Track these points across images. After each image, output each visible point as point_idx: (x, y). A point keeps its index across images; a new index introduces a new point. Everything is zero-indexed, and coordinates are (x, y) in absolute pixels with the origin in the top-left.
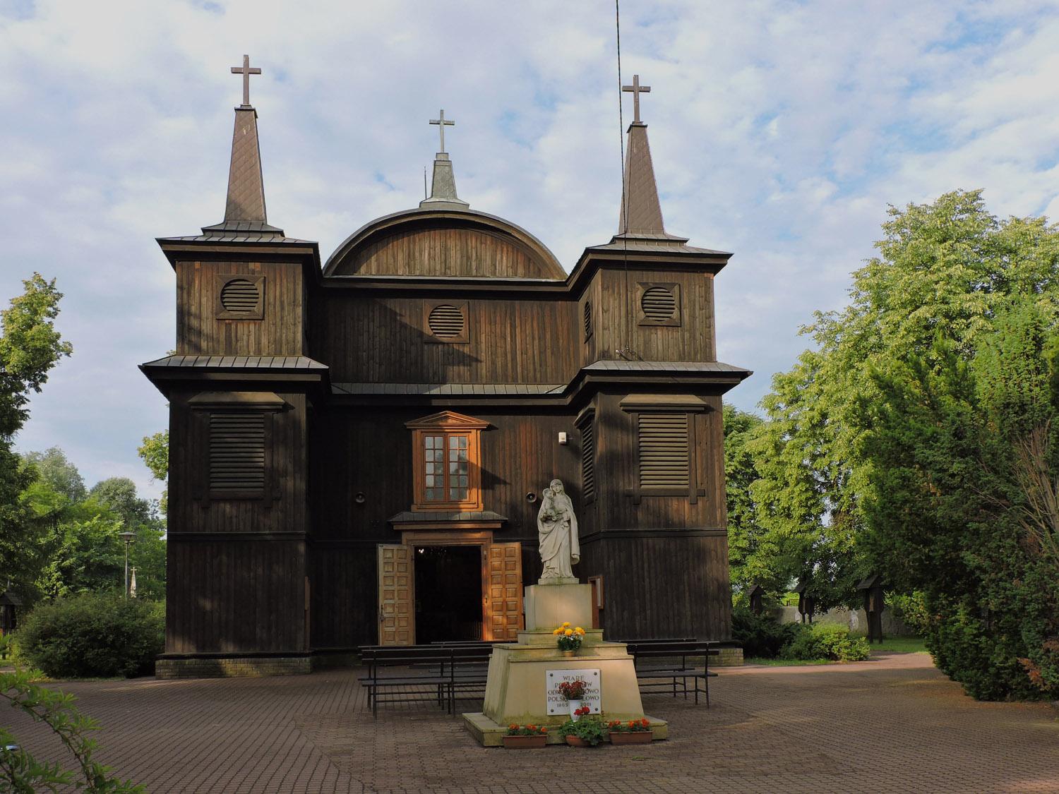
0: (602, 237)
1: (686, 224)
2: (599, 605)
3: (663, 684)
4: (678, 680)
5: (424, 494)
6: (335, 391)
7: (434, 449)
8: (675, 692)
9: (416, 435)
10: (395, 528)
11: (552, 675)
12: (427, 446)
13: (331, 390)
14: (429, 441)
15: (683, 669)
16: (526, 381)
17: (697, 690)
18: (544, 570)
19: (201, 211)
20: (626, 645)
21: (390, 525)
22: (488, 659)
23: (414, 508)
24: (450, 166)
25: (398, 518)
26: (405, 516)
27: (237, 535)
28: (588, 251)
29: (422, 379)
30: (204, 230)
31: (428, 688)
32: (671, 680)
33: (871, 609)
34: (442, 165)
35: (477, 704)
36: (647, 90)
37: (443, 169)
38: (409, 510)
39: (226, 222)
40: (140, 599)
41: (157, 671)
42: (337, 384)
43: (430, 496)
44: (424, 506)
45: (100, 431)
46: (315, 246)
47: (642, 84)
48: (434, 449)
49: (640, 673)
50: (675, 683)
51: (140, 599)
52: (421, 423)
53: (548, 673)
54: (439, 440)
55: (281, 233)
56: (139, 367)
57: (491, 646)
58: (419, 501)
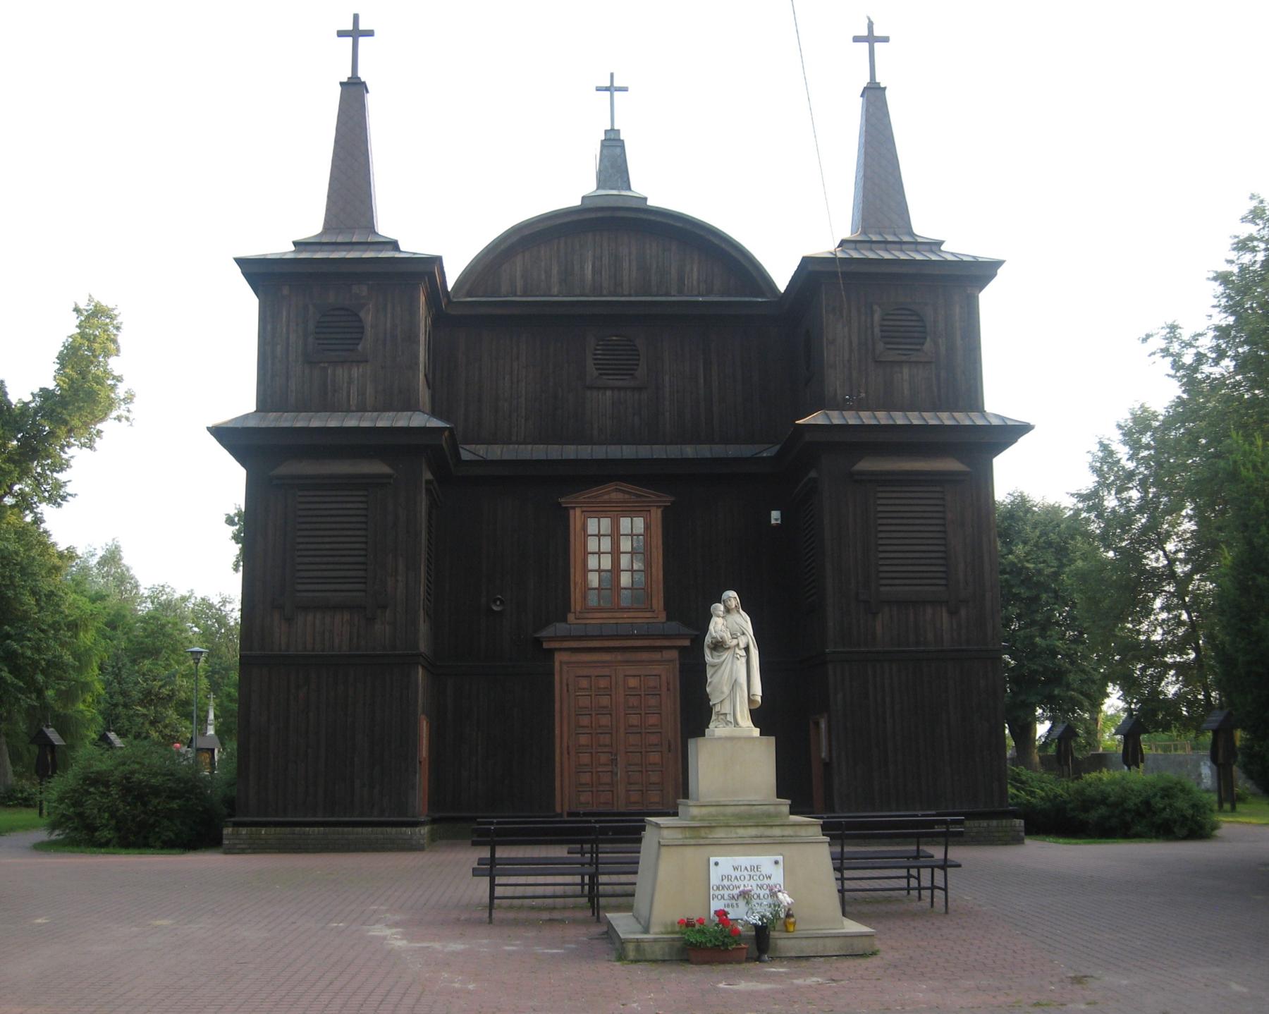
0: (824, 244)
1: (942, 217)
2: (823, 755)
3: (864, 880)
4: (914, 872)
5: (585, 598)
6: (465, 455)
7: (632, 535)
8: (909, 889)
9: (576, 516)
10: (545, 645)
11: (716, 864)
12: (590, 531)
13: (459, 453)
14: (592, 526)
15: (917, 857)
16: (725, 441)
17: (933, 888)
18: (714, 717)
19: (292, 217)
20: (821, 821)
21: (538, 642)
22: (639, 841)
23: (571, 617)
24: (623, 147)
25: (544, 633)
26: (560, 628)
27: (332, 656)
28: (806, 261)
29: (952, 408)
30: (295, 244)
31: (568, 879)
32: (903, 872)
33: (1221, 760)
34: (613, 147)
35: (625, 900)
36: (370, 33)
37: (613, 155)
38: (565, 620)
39: (328, 226)
40: (206, 745)
41: (226, 842)
42: (467, 447)
43: (593, 600)
44: (586, 615)
45: (158, 519)
46: (436, 261)
47: (363, 26)
48: (632, 535)
49: (840, 864)
50: (909, 877)
51: (206, 745)
52: (581, 499)
53: (713, 860)
54: (606, 523)
55: (394, 245)
56: (208, 429)
57: (643, 821)
58: (578, 609)
